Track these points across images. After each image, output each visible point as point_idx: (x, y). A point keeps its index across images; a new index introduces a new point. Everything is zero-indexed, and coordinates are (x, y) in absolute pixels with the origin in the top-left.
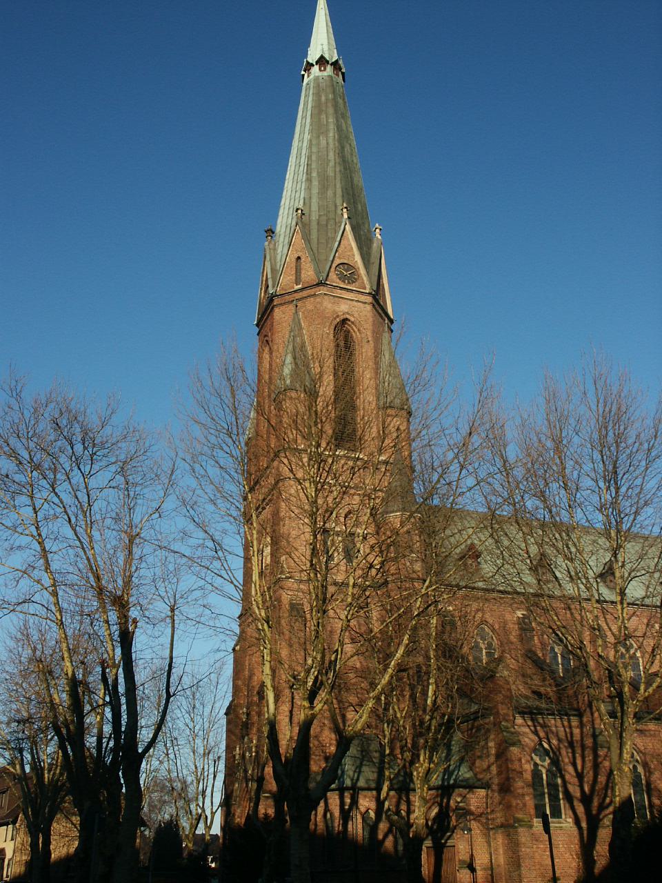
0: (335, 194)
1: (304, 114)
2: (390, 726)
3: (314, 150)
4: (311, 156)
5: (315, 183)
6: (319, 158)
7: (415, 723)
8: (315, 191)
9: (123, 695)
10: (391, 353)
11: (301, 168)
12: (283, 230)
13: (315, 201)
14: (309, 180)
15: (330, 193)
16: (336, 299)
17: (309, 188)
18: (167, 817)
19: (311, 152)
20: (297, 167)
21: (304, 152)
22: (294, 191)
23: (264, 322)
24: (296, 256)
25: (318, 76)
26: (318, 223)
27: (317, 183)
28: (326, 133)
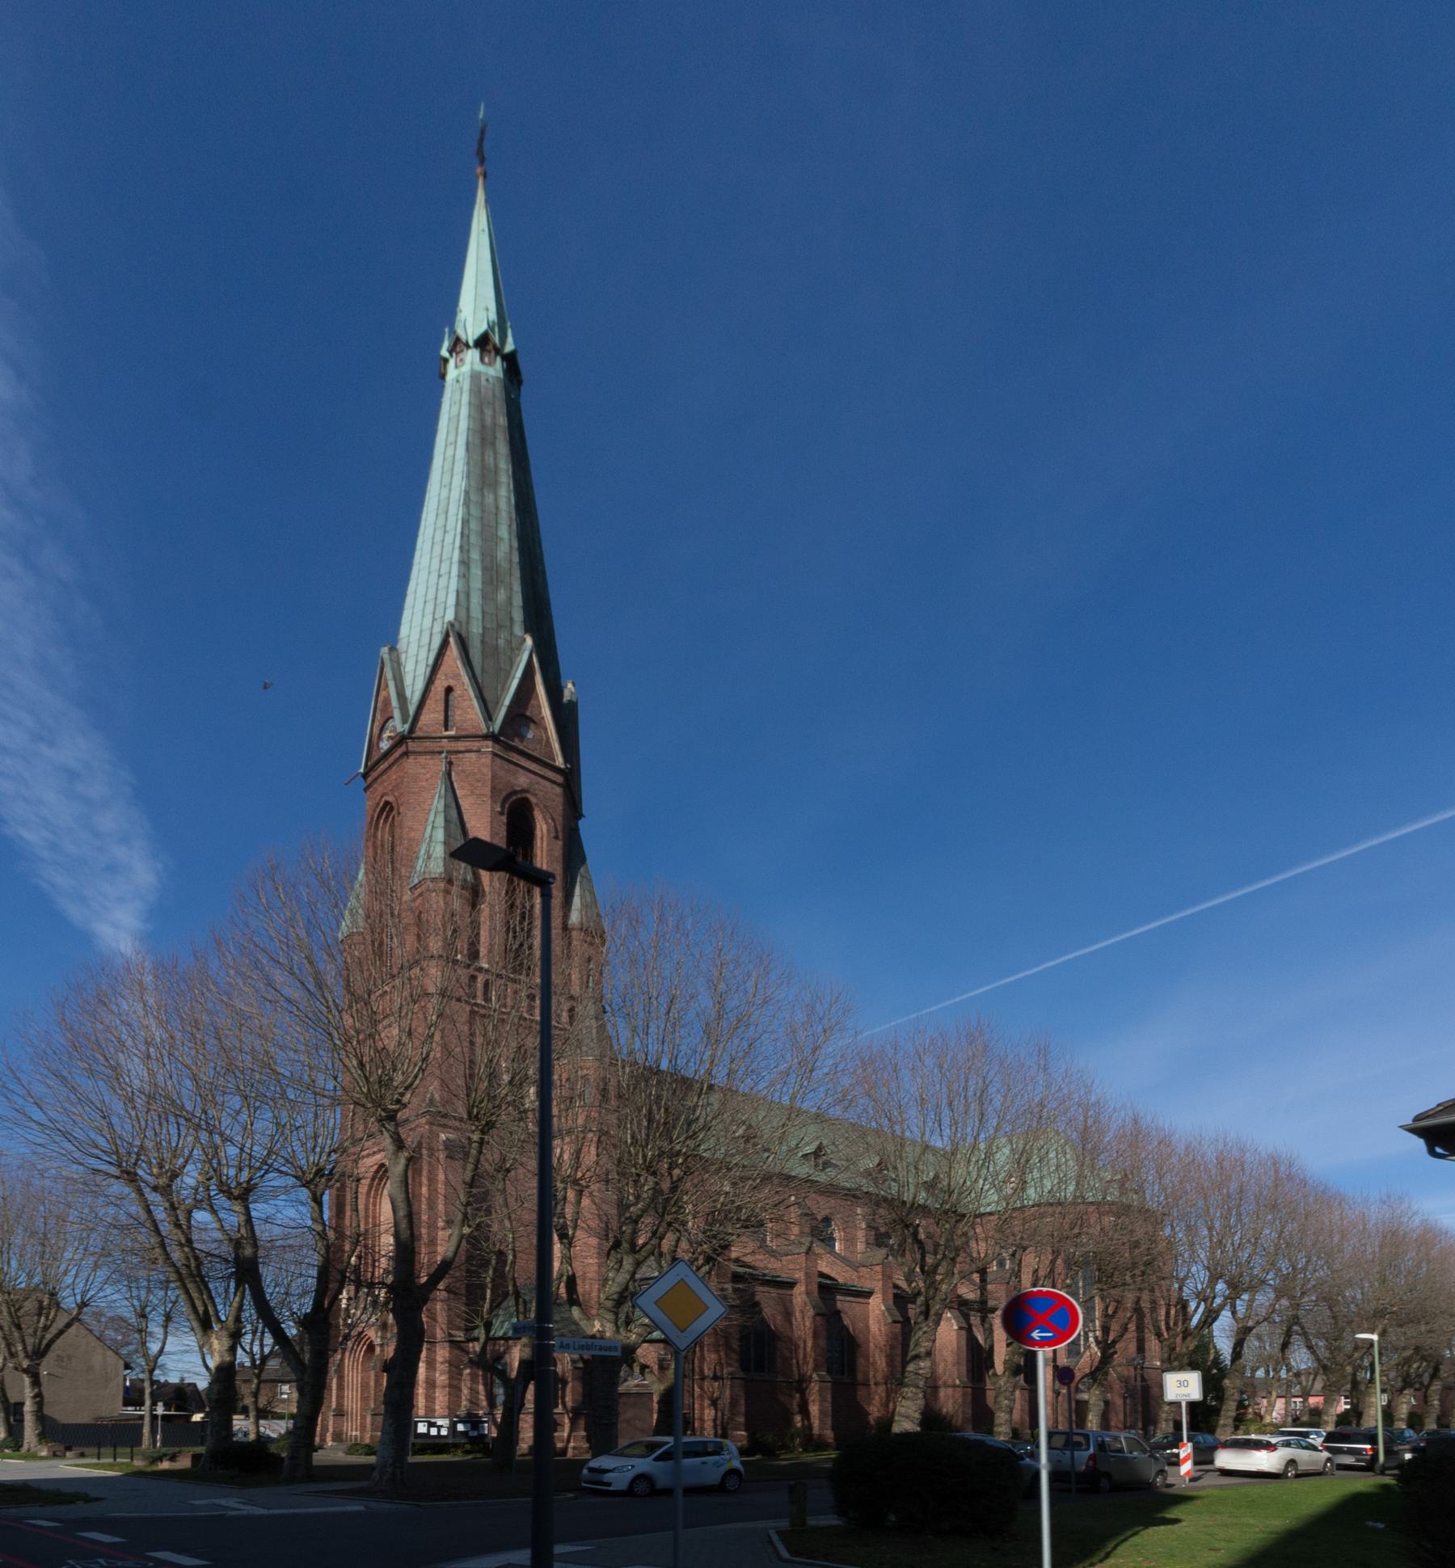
0: (510, 599)
1: (451, 439)
2: (1112, 1351)
3: (474, 511)
4: (468, 521)
5: (476, 571)
6: (482, 533)
7: (435, 1222)
8: (476, 584)
9: (386, 1231)
10: (357, 1211)
11: (449, 538)
12: (415, 636)
13: (476, 600)
14: (465, 563)
15: (502, 595)
16: (512, 767)
17: (464, 576)
18: (797, 1276)
19: (469, 514)
20: (439, 534)
21: (453, 510)
22: (434, 575)
23: (390, 767)
24: (446, 684)
25: (480, 373)
26: (483, 642)
27: (480, 573)
28: (494, 486)
